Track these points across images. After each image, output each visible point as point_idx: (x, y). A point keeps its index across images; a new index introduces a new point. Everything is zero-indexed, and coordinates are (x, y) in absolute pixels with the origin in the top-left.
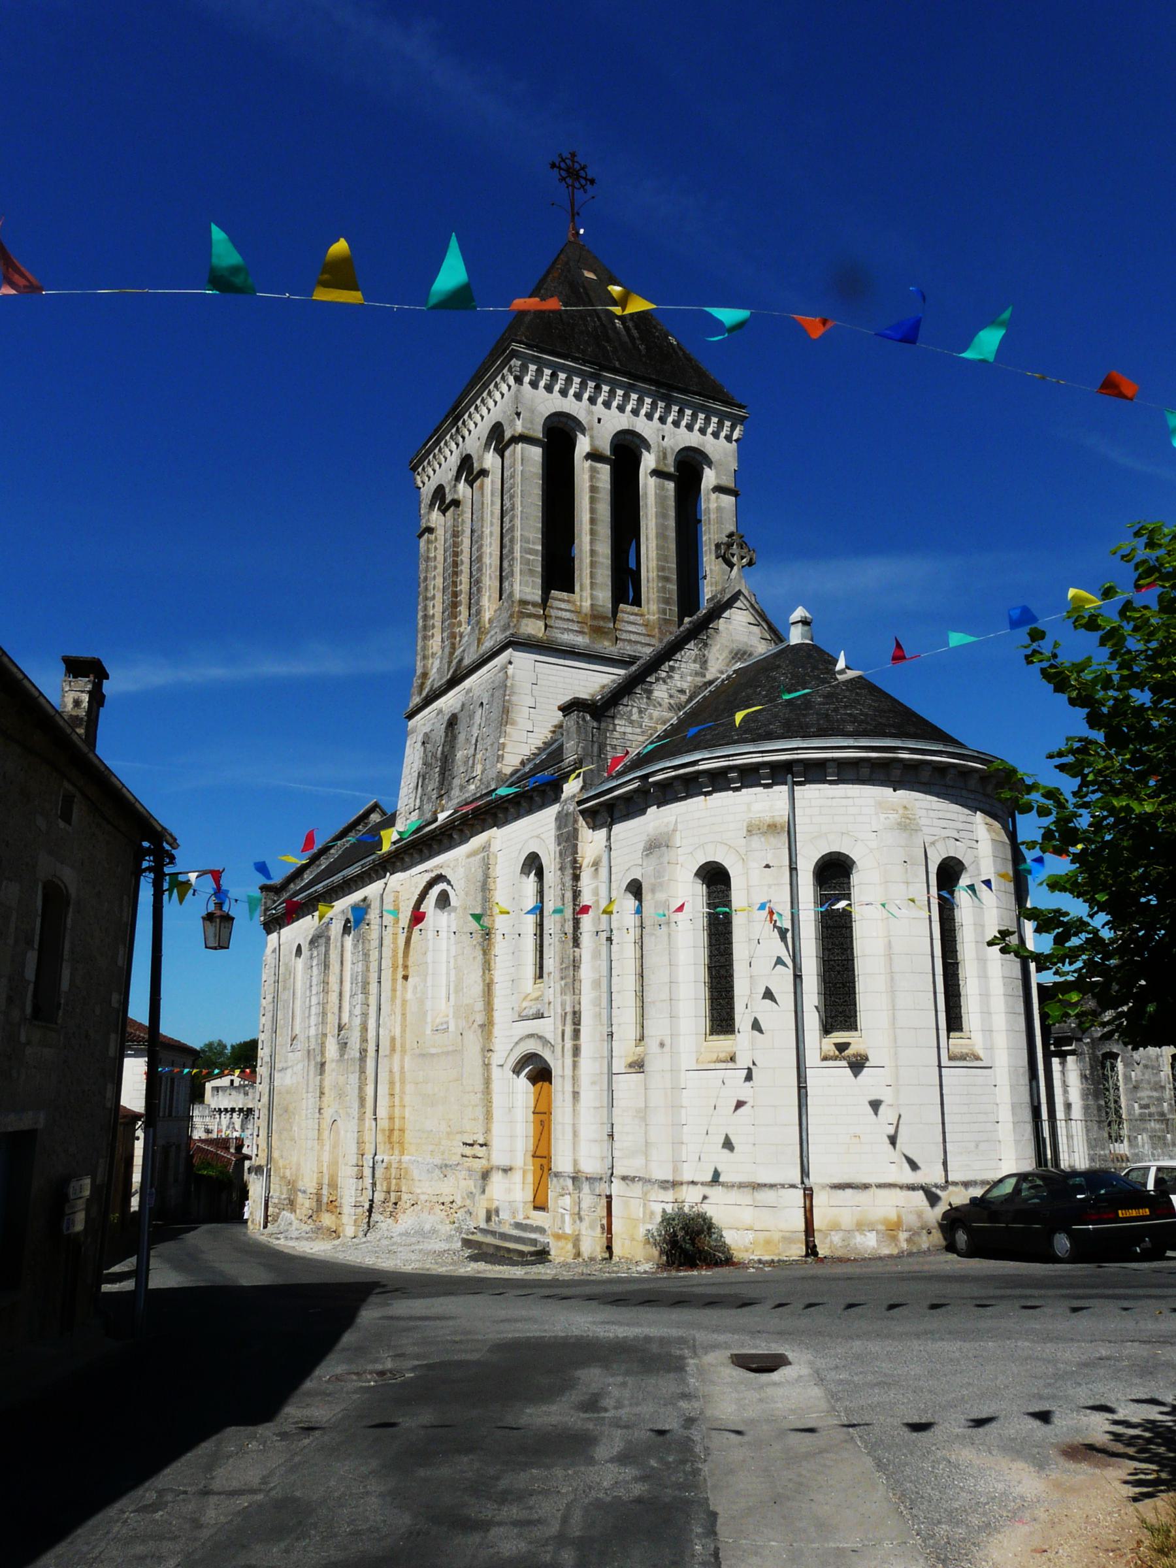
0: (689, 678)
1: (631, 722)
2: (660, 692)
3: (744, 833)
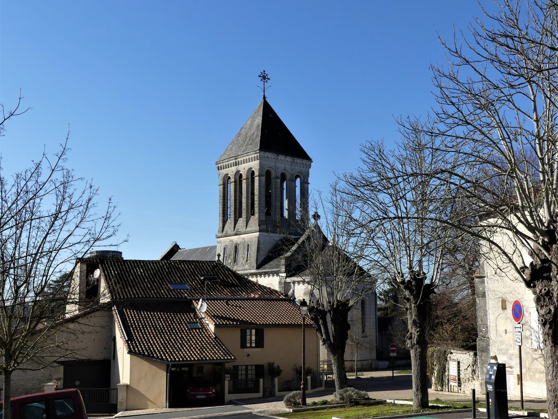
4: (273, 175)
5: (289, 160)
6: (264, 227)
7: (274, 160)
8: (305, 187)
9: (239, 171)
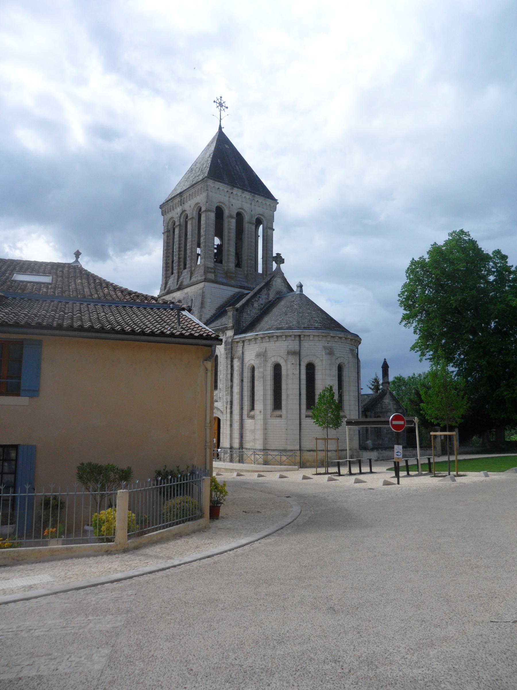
0: (264, 300)
1: (248, 314)
2: (256, 305)
3: (286, 353)
4: (226, 213)
5: (248, 197)
6: (211, 276)
7: (228, 195)
8: (269, 233)
9: (185, 211)
